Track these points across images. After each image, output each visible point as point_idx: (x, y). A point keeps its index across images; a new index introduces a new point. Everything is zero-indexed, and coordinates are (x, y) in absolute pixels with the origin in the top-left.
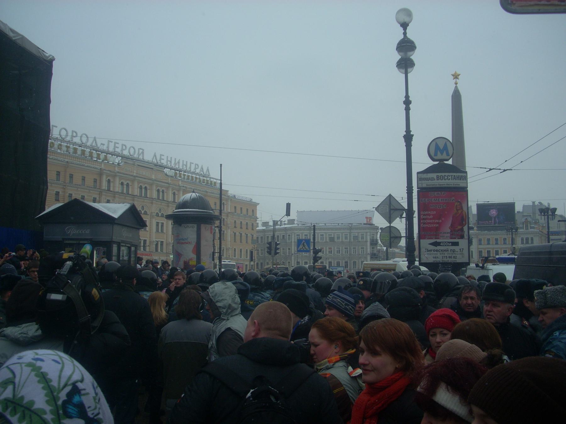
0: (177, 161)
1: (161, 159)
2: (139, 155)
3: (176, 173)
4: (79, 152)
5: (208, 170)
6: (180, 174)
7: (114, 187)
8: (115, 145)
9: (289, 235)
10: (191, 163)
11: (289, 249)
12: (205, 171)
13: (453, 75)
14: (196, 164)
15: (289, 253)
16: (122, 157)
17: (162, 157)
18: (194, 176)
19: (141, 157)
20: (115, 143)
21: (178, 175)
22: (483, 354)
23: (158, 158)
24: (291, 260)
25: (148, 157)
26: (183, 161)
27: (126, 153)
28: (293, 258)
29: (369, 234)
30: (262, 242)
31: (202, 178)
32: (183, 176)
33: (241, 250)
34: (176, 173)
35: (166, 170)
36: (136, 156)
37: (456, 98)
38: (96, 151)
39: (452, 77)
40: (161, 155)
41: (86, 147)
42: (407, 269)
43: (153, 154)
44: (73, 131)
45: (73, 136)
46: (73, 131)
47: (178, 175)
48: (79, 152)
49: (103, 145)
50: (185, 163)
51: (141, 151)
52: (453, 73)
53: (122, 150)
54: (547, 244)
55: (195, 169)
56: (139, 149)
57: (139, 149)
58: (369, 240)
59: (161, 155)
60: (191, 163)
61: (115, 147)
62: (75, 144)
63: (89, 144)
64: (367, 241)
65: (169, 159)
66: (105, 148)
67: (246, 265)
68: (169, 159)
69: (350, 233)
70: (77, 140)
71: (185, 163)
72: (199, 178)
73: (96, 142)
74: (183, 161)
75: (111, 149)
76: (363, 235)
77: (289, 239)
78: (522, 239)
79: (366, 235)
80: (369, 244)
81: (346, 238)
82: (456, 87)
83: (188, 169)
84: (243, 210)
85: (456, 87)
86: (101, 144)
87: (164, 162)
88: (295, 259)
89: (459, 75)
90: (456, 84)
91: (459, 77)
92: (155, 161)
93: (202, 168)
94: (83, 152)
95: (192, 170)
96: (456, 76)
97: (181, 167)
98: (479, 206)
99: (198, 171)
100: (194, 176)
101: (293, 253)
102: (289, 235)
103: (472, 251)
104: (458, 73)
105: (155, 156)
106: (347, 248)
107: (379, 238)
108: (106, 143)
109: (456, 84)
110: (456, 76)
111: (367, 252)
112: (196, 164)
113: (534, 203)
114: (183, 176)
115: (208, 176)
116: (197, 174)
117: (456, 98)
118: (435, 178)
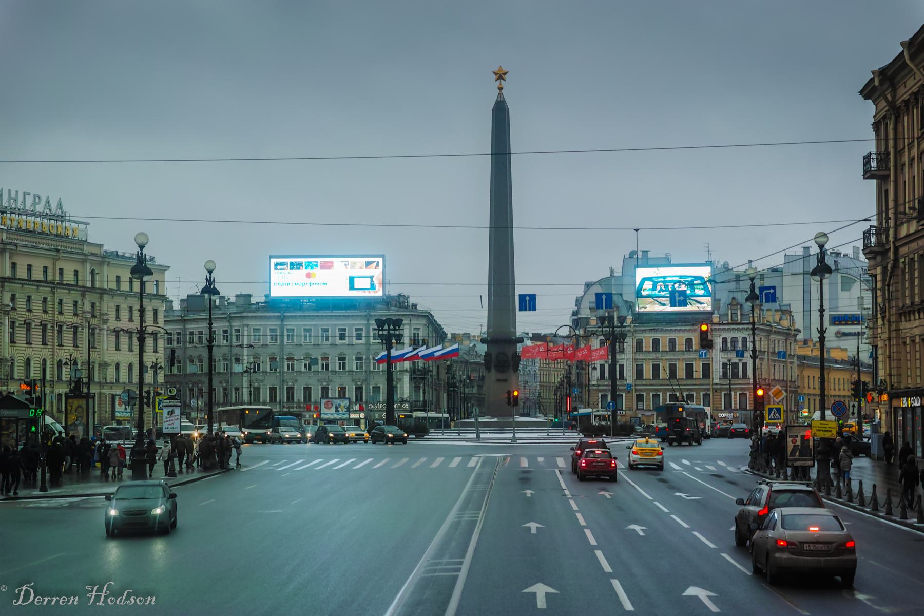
5: (60, 205)
9: (238, 331)
12: (54, 206)
13: (496, 74)
14: (35, 196)
22: (610, 570)
26: (9, 191)
33: (28, 360)
37: (500, 115)
39: (495, 77)
50: (13, 195)
52: (496, 69)
55: (34, 204)
60: (25, 194)
67: (201, 333)
71: (13, 195)
74: (9, 191)
78: (725, 340)
81: (359, 337)
82: (500, 95)
85: (500, 95)
90: (501, 89)
91: (506, 77)
93: (48, 202)
96: (500, 76)
98: (520, 296)
99: (39, 208)
103: (621, 366)
104: (505, 69)
106: (327, 359)
109: (501, 89)
110: (500, 76)
112: (35, 196)
114: (8, 222)
115: (61, 218)
116: (42, 215)
117: (500, 115)
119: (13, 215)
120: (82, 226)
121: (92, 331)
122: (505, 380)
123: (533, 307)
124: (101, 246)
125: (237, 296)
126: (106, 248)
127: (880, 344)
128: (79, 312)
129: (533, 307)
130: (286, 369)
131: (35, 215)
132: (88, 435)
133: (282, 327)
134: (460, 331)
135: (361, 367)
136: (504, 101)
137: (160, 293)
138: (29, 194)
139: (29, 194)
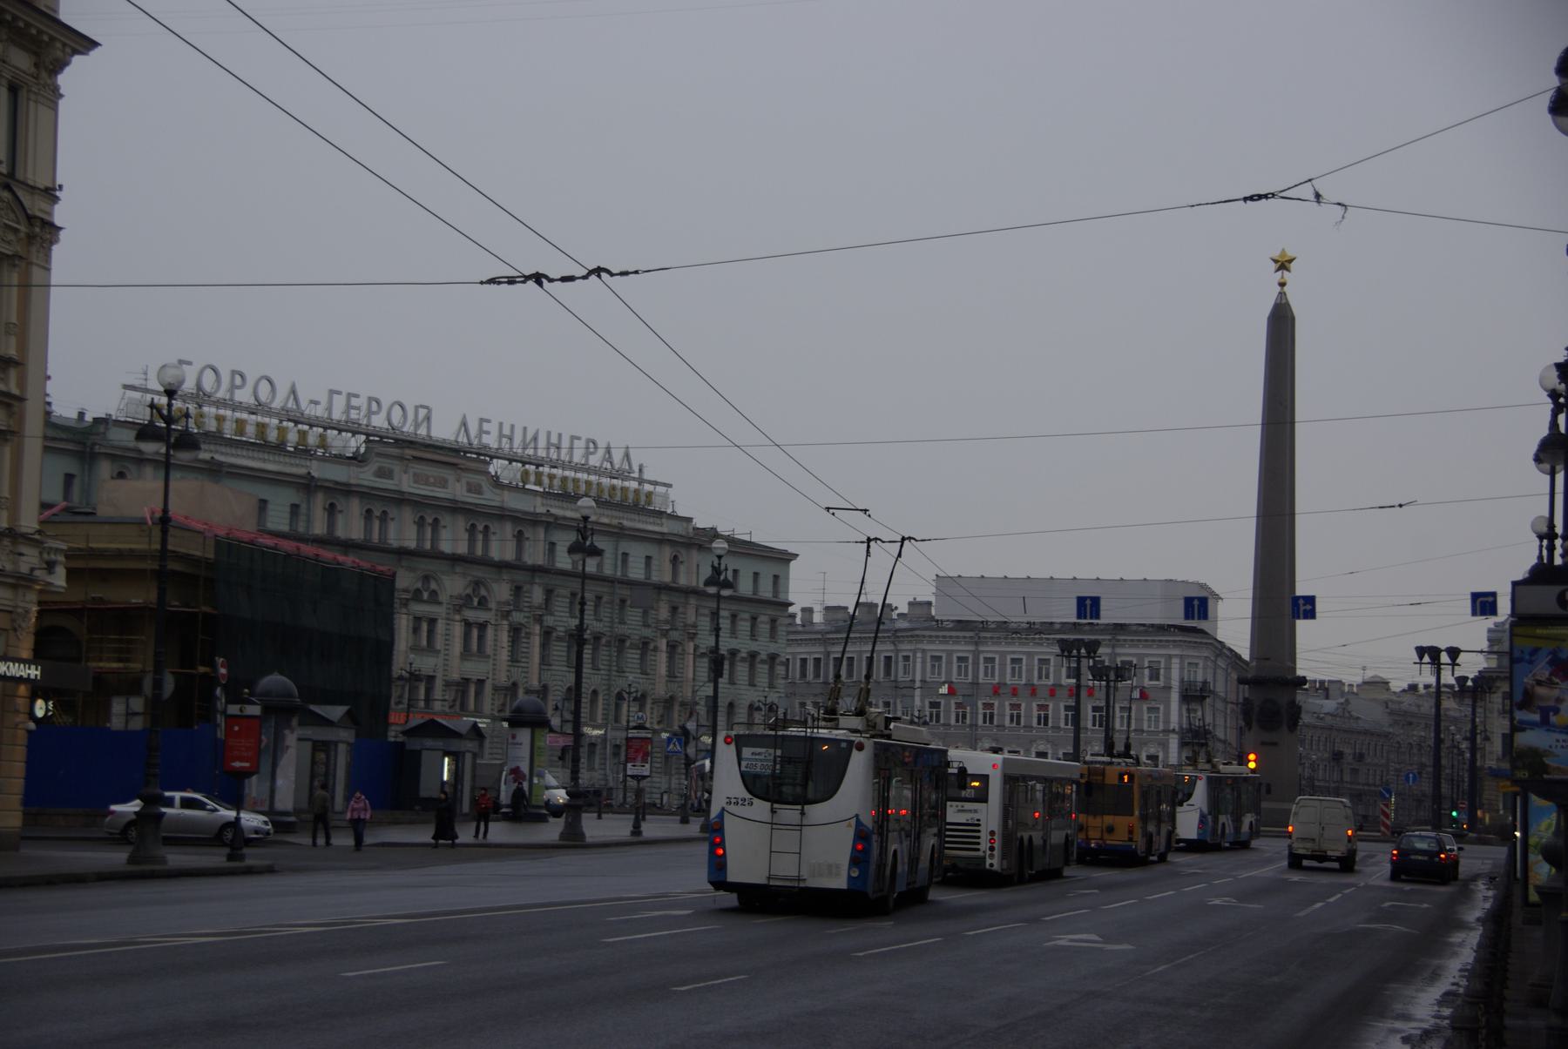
0: (529, 436)
1: (481, 432)
2: (417, 425)
3: (526, 474)
4: (250, 430)
6: (539, 475)
7: (309, 521)
8: (348, 401)
9: (906, 658)
10: (573, 438)
12: (617, 456)
13: (1276, 261)
16: (368, 435)
17: (486, 426)
19: (422, 431)
20: (350, 395)
21: (532, 478)
23: (473, 431)
25: (443, 430)
26: (549, 433)
27: (379, 421)
29: (1175, 663)
30: (817, 675)
32: (546, 481)
34: (526, 474)
35: (496, 466)
36: (408, 428)
37: (1281, 323)
38: (296, 423)
39: (1274, 266)
40: (482, 420)
41: (269, 413)
43: (458, 420)
44: (234, 373)
45: (233, 387)
46: (234, 373)
47: (532, 478)
48: (250, 430)
49: (316, 403)
51: (422, 413)
52: (1276, 255)
53: (370, 413)
55: (587, 454)
56: (417, 408)
57: (417, 408)
58: (1175, 683)
59: (482, 420)
60: (573, 438)
61: (349, 407)
62: (236, 407)
63: (277, 404)
64: (1168, 688)
65: (506, 431)
66: (319, 411)
68: (506, 431)
69: (976, 654)
70: (244, 396)
73: (296, 399)
74: (549, 433)
75: (337, 415)
76: (1047, 661)
79: (1168, 668)
80: (1175, 697)
82: (1282, 294)
83: (564, 456)
85: (1282, 294)
86: (312, 402)
87: (491, 441)
89: (1291, 261)
90: (1282, 285)
92: (463, 439)
93: (608, 450)
94: (261, 427)
95: (578, 458)
96: (1283, 265)
97: (542, 453)
99: (595, 461)
102: (906, 658)
104: (1290, 254)
105: (464, 424)
108: (323, 398)
109: (1282, 285)
110: (1283, 265)
111: (1167, 722)
112: (589, 441)
114: (546, 481)
117: (1281, 323)
118: (177, 802)
119: (554, 471)
120: (660, 489)
121: (672, 647)
122: (1275, 744)
123: (1096, 601)
124: (689, 520)
125: (910, 604)
126: (700, 523)
127: (422, 704)
128: (650, 621)
129: (1096, 601)
130: (980, 722)
131: (589, 470)
132: (170, 841)
133: (976, 654)
134: (1326, 676)
135: (964, 717)
136: (1287, 304)
137: (782, 598)
138: (339, 393)
139: (339, 393)
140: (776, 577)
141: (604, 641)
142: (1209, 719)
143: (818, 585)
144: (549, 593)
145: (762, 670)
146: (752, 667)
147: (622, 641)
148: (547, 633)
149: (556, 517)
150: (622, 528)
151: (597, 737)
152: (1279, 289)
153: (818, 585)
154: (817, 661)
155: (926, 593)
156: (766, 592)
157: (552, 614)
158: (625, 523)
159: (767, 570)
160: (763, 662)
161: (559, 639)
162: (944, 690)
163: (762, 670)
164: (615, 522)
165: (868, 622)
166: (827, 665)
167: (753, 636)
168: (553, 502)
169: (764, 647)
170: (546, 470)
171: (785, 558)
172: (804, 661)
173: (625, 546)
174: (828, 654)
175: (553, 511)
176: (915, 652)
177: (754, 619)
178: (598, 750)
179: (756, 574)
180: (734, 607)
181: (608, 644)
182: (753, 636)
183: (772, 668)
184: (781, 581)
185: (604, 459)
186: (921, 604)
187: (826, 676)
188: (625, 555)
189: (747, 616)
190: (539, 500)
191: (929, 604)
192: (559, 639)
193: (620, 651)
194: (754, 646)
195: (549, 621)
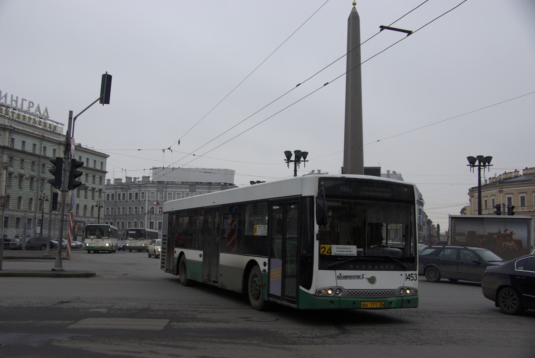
9: (143, 193)
10: (23, 100)
11: (142, 208)
12: (42, 111)
15: (142, 211)
18: (32, 117)
24: (144, 220)
26: (12, 96)
28: (146, 218)
30: (113, 199)
31: (38, 119)
42: (460, 214)
54: (185, 251)
55: (29, 107)
60: (23, 100)
72: (34, 119)
74: (12, 96)
77: (143, 197)
82: (354, 8)
84: (97, 162)
85: (354, 8)
88: (148, 219)
93: (38, 107)
95: (25, 108)
96: (354, 4)
97: (8, 103)
99: (32, 110)
100: (32, 117)
101: (146, 212)
102: (143, 193)
107: (316, 243)
110: (354, 4)
112: (30, 102)
113: (388, 171)
116: (32, 114)
120: (59, 125)
137: (104, 170)
140: (102, 163)
141: (35, 179)
142: (45, 232)
143: (115, 171)
144: (11, 158)
145: (97, 194)
146: (93, 193)
147: (43, 180)
148: (10, 174)
149: (14, 128)
150: (44, 136)
151: (32, 216)
152: (353, 6)
153: (115, 171)
154: (113, 195)
155: (148, 173)
156: (98, 167)
157: (12, 167)
158: (45, 135)
159: (99, 160)
160: (97, 191)
161: (15, 177)
162: (155, 203)
163: (97, 194)
164: (41, 134)
165: (130, 184)
166: (116, 196)
167: (94, 183)
168: (13, 122)
169: (98, 187)
170: (11, 110)
171: (105, 156)
172: (108, 195)
173: (45, 144)
174: (116, 192)
175: (13, 125)
176: (146, 191)
177: (94, 176)
178: (32, 222)
179: (95, 161)
180: (87, 172)
181: (37, 180)
182: (94, 183)
183: (100, 194)
184: (104, 164)
185: (36, 110)
186: (146, 177)
187: (116, 200)
188: (45, 147)
189: (91, 175)
190: (7, 120)
191: (149, 177)
192: (15, 177)
193: (42, 184)
194: (94, 186)
195: (11, 169)
